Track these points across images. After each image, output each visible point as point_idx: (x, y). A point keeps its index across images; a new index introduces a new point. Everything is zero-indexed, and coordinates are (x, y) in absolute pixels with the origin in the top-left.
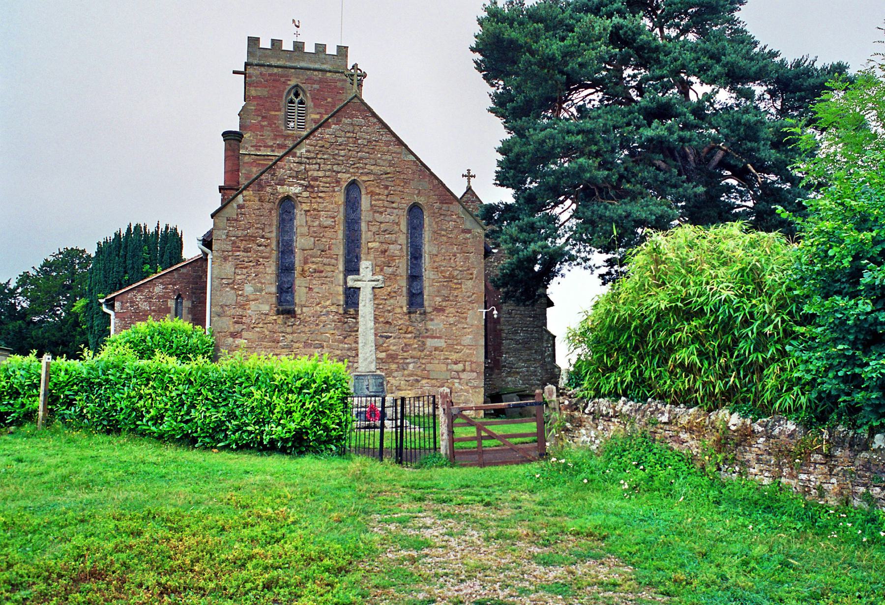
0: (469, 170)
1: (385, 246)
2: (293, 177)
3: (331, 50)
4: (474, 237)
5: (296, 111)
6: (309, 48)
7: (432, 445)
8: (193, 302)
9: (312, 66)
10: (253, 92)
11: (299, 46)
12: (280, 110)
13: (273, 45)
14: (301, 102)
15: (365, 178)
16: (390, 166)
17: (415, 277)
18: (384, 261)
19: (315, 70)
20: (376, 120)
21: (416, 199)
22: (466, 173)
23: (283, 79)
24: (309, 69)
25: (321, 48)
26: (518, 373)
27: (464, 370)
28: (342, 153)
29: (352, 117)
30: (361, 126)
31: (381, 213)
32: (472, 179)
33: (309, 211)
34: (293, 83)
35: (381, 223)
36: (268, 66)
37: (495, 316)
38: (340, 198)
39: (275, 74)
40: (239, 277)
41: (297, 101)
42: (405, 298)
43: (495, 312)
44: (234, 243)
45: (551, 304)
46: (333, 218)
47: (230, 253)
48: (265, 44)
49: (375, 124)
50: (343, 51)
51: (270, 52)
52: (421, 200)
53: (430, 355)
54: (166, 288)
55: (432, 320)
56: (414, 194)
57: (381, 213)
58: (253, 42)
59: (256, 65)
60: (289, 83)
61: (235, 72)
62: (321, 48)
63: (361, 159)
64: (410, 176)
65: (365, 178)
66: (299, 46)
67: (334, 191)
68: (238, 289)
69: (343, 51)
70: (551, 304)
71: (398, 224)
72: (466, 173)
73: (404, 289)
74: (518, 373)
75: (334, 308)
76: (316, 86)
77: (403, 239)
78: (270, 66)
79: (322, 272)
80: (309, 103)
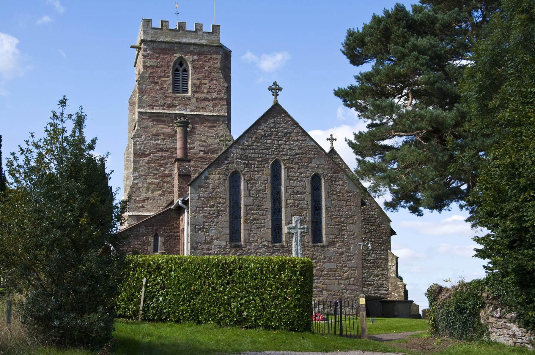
0: (331, 135)
1: (297, 202)
2: (239, 159)
4: (355, 195)
6: (190, 27)
7: (333, 333)
8: (165, 239)
11: (182, 26)
16: (299, 150)
19: (195, 44)
20: (289, 119)
21: (316, 170)
22: (329, 137)
24: (190, 44)
25: (199, 27)
26: (371, 285)
27: (349, 284)
28: (269, 141)
29: (274, 117)
30: (280, 123)
31: (294, 180)
32: (334, 142)
33: (249, 180)
35: (294, 187)
36: (159, 42)
38: (268, 171)
39: (164, 49)
40: (206, 224)
41: (181, 69)
42: (311, 236)
45: (393, 233)
46: (265, 184)
47: (201, 209)
49: (288, 121)
52: (320, 171)
53: (327, 274)
56: (315, 167)
57: (294, 180)
61: (132, 47)
63: (281, 145)
64: (312, 156)
65: (284, 158)
66: (182, 26)
67: (264, 167)
68: (206, 232)
69: (216, 28)
70: (393, 233)
71: (305, 187)
74: (371, 285)
75: (266, 243)
76: (196, 57)
77: (308, 197)
78: (161, 42)
79: (258, 220)
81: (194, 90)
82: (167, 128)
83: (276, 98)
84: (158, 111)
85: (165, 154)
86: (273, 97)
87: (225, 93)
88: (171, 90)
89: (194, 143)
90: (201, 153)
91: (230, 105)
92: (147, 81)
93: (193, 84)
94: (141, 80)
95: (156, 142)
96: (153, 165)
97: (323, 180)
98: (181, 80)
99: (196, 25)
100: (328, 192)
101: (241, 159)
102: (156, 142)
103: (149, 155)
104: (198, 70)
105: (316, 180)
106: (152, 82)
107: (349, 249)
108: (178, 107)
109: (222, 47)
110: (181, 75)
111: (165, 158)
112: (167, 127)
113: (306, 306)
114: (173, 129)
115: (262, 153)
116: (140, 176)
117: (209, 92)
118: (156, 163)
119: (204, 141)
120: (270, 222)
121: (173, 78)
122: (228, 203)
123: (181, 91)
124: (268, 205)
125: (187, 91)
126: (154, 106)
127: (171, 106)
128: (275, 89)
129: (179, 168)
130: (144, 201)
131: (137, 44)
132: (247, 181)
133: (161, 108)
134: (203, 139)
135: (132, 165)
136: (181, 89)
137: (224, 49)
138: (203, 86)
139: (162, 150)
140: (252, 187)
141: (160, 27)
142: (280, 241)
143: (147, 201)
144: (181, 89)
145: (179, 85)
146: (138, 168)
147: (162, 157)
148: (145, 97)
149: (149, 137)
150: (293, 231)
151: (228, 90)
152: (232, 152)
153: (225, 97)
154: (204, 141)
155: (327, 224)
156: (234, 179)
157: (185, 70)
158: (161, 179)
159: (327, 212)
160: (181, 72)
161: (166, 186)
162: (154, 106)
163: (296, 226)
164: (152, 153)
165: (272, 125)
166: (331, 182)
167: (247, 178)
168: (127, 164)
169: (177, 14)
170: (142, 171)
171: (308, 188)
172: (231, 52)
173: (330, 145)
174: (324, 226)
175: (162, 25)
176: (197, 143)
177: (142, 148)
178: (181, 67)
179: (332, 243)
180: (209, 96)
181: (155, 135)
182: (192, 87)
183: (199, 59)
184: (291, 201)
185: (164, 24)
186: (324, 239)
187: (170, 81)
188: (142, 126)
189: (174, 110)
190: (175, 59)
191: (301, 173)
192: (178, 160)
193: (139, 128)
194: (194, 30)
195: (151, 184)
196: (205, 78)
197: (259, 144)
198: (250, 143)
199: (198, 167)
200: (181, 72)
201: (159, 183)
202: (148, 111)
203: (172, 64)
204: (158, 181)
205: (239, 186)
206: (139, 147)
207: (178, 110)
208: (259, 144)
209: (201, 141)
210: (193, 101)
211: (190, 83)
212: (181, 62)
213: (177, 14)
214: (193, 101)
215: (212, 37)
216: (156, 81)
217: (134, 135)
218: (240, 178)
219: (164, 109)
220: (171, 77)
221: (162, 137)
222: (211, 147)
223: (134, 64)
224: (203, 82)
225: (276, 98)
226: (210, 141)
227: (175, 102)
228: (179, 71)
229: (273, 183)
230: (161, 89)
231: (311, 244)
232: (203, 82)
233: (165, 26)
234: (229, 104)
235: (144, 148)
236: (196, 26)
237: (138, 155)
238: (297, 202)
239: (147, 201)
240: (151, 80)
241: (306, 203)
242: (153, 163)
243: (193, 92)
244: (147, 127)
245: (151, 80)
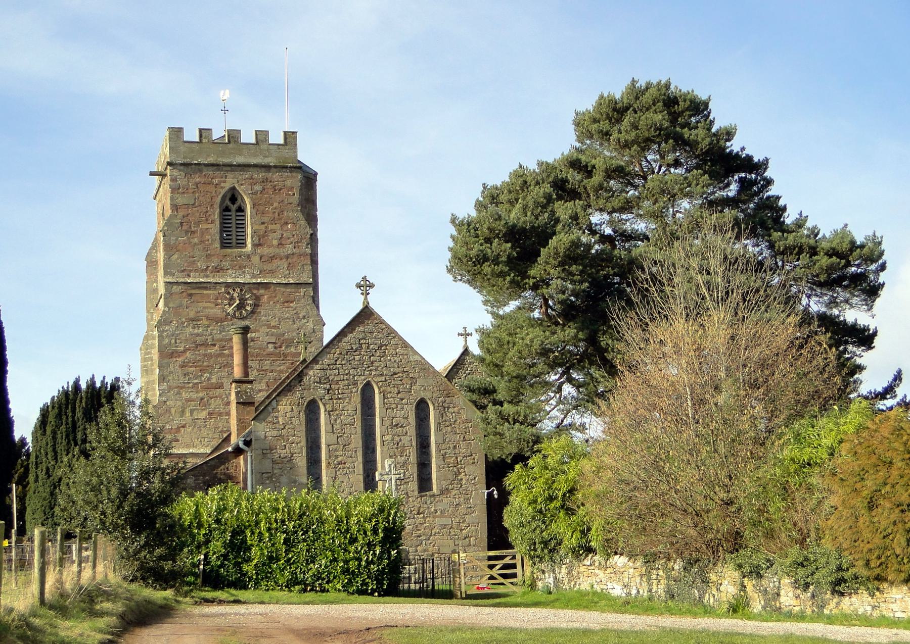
3: (276, 138)
5: (233, 221)
6: (248, 137)
9: (253, 161)
10: (180, 200)
17: (424, 466)
18: (397, 449)
21: (422, 395)
25: (262, 136)
32: (469, 338)
37: (496, 496)
38: (357, 399)
41: (234, 208)
43: (495, 492)
48: (191, 135)
50: (290, 138)
55: (181, 515)
58: (176, 133)
59: (181, 164)
61: (152, 174)
69: (290, 138)
71: (407, 418)
73: (415, 475)
77: (412, 430)
81: (257, 242)
82: (212, 308)
83: (366, 299)
84: (197, 280)
85: (212, 351)
86: (363, 297)
87: (308, 244)
88: (217, 245)
89: (258, 331)
90: (270, 346)
91: (317, 264)
92: (177, 228)
93: (254, 232)
94: (168, 229)
95: (196, 331)
96: (192, 369)
97: (431, 407)
98: (234, 225)
99: (257, 133)
100: (439, 424)
101: (320, 383)
102: (196, 331)
103: (184, 351)
104: (261, 208)
105: (422, 407)
106: (187, 232)
107: (469, 499)
108: (230, 272)
109: (300, 168)
110: (233, 217)
111: (210, 356)
112: (213, 305)
113: (396, 566)
114: (223, 308)
115: (349, 374)
116: (170, 388)
117: (280, 244)
118: (196, 367)
119: (275, 327)
120: (361, 466)
121: (221, 223)
122: (304, 443)
123: (234, 244)
124: (357, 441)
125: (243, 244)
126: (191, 271)
127: (218, 270)
128: (365, 286)
129: (237, 393)
130: (178, 430)
131: (160, 169)
132: (329, 413)
133: (202, 274)
134: (273, 324)
135: (157, 371)
136: (234, 241)
137: (304, 172)
138: (271, 235)
139: (205, 344)
140: (336, 420)
141: (197, 140)
142: (320, 489)
143: (182, 430)
144: (234, 241)
145: (230, 236)
146: (167, 376)
147: (205, 355)
148: (175, 256)
149: (183, 323)
150: (385, 477)
151: (313, 240)
152: (307, 374)
153: (309, 251)
154: (275, 327)
155: (438, 466)
156: (312, 409)
157: (241, 210)
158: (204, 393)
159: (439, 450)
160: (233, 213)
161: (214, 404)
162: (191, 271)
163: (390, 470)
164: (189, 349)
165: (361, 336)
166: (443, 410)
167: (329, 407)
168: (145, 366)
169: (225, 110)
170: (174, 379)
171: (412, 419)
172: (316, 174)
173: (463, 343)
174: (434, 470)
175: (201, 136)
176: (264, 330)
177: (173, 341)
178: (233, 203)
179: (444, 492)
180: (283, 251)
181: (192, 320)
182: (252, 238)
183: (264, 189)
184: (389, 437)
185: (204, 135)
186: (435, 487)
187: (215, 228)
188: (171, 305)
189: (222, 277)
190: (223, 192)
191: (402, 399)
192: (236, 381)
193: (167, 309)
194: (253, 141)
195: (188, 400)
196: (273, 221)
197: (344, 362)
198: (333, 362)
199: (266, 371)
200: (233, 213)
201: (202, 399)
202: (181, 280)
203: (219, 199)
204: (201, 395)
205: (318, 419)
206: (167, 341)
207: (230, 275)
208: (344, 362)
209: (269, 326)
210: (255, 259)
211: (249, 230)
212: (233, 196)
213: (225, 110)
214: (255, 259)
215: (286, 152)
216: (193, 229)
217: (159, 321)
218: (319, 408)
219: (207, 276)
220: (218, 223)
221: (205, 322)
222: (286, 336)
223: (153, 195)
224: (270, 227)
225: (366, 299)
226: (283, 328)
227: (226, 264)
228: (230, 211)
229: (364, 413)
230: (202, 242)
231: (416, 493)
232: (270, 227)
233: (206, 138)
234: (314, 262)
235: (176, 343)
236: (256, 135)
237: (167, 354)
238: (397, 439)
239: (182, 430)
240: (185, 227)
241: (409, 439)
242: (191, 367)
243: (256, 246)
244: (180, 306)
245: (185, 227)
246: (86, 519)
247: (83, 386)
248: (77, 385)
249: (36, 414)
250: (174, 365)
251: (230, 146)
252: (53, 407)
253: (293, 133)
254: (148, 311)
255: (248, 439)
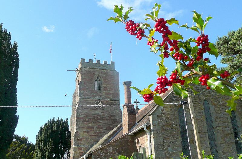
12: (93, 83)
13: (90, 61)
14: (99, 81)
15: (210, 98)
19: (104, 69)
22: (135, 101)
23: (93, 73)
25: (106, 62)
34: (97, 74)
41: (98, 80)
44: (162, 127)
51: (89, 64)
54: (114, 149)
58: (83, 60)
60: (95, 74)
62: (106, 62)
65: (210, 98)
72: (138, 101)
80: (102, 81)
148: (82, 91)
246: (168, 139)
247: (56, 120)
248: (53, 120)
249: (39, 129)
250: (81, 121)
251: (97, 64)
252: (45, 127)
253: (114, 62)
254: (73, 109)
255: (148, 125)
